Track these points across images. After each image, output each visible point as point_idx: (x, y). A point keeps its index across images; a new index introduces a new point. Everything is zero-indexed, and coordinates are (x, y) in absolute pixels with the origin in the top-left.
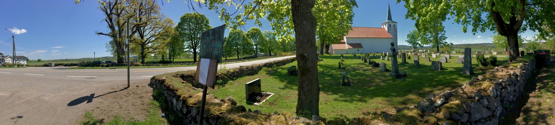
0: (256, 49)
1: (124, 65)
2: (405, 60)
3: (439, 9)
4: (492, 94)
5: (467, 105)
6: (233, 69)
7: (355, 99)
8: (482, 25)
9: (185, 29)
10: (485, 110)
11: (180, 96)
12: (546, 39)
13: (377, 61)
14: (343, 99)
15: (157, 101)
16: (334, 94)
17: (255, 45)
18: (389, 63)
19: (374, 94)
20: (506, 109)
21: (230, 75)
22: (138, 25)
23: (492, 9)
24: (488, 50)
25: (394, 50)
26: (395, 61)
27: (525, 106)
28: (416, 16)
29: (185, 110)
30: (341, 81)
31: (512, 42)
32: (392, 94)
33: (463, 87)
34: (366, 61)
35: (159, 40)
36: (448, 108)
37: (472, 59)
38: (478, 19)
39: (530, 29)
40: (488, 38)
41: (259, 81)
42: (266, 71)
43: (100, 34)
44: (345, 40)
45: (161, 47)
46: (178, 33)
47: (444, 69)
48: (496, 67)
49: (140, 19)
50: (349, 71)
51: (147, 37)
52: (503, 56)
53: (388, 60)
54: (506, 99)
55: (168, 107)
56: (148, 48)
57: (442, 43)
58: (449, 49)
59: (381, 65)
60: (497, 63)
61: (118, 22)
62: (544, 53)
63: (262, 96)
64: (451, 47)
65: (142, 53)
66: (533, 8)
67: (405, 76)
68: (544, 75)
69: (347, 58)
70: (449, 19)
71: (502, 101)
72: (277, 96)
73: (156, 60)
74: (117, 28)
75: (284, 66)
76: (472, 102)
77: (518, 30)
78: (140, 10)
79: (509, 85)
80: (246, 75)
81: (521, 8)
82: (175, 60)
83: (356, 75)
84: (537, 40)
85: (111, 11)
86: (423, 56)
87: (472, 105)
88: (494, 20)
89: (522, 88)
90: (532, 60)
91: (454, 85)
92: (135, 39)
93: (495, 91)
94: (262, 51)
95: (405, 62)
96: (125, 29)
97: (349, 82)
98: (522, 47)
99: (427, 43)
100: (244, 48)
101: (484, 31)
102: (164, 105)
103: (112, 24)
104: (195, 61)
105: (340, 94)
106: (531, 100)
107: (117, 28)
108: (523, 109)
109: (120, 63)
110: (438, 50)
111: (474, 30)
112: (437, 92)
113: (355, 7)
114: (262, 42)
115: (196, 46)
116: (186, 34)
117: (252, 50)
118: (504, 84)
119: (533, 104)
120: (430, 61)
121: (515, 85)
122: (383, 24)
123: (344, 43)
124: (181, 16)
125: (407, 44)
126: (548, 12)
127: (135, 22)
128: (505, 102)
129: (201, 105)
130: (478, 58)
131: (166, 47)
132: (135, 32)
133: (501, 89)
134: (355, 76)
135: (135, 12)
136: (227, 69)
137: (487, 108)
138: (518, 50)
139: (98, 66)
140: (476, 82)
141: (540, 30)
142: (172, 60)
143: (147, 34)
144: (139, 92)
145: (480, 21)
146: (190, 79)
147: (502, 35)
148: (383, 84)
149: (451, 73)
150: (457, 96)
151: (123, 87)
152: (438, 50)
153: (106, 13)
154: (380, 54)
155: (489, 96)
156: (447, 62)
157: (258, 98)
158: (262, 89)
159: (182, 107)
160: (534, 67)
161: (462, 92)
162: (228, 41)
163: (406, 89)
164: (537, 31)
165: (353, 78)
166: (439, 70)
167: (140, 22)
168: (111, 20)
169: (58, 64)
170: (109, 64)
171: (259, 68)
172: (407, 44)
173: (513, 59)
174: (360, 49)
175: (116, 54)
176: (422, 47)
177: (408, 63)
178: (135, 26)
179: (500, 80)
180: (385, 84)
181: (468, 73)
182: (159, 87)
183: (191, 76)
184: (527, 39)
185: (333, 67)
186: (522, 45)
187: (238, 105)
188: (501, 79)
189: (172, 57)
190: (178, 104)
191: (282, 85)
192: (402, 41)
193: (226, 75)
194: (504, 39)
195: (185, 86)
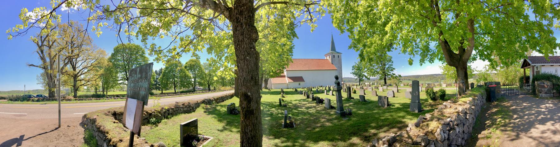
0: (195, 82)
1: (56, 100)
2: (350, 94)
3: (384, 40)
4: (439, 138)
8: (431, 55)
11: (110, 140)
12: (496, 70)
13: (321, 96)
16: (275, 138)
18: (333, 99)
21: (165, 113)
22: (70, 56)
23: (439, 39)
24: (438, 82)
25: (338, 84)
26: (340, 97)
28: (360, 46)
30: (283, 121)
31: (462, 73)
32: (337, 137)
33: (408, 129)
34: (308, 97)
35: (92, 72)
37: (421, 93)
38: (427, 49)
39: (480, 59)
40: (437, 67)
41: (195, 122)
42: (203, 108)
43: (30, 65)
44: (285, 73)
45: (94, 79)
46: (111, 64)
49: (72, 51)
50: (290, 109)
51: (80, 69)
52: (452, 90)
54: (454, 143)
56: (81, 80)
57: (389, 75)
58: (397, 82)
59: (326, 101)
62: (494, 85)
63: (198, 140)
64: (399, 78)
65: (74, 86)
66: (483, 38)
67: (350, 114)
68: (495, 110)
69: (287, 93)
70: (396, 49)
72: (217, 141)
73: (89, 93)
74: (48, 60)
75: (222, 104)
77: (468, 60)
79: (457, 125)
80: (182, 113)
81: (471, 36)
82: (109, 93)
85: (42, 42)
86: (369, 89)
88: (443, 49)
89: (471, 128)
90: (482, 94)
91: (399, 125)
92: (66, 71)
93: (442, 133)
94: (200, 84)
95: (350, 98)
96: (57, 61)
97: (291, 123)
98: (472, 78)
100: (181, 81)
101: (433, 61)
103: (44, 56)
107: (48, 60)
109: (51, 97)
110: (385, 83)
111: (422, 61)
112: (382, 135)
114: (201, 75)
116: (119, 65)
117: (190, 83)
118: (451, 123)
120: (377, 95)
121: (464, 125)
122: (326, 55)
123: (284, 76)
126: (497, 43)
127: (68, 54)
130: (427, 92)
131: (99, 79)
132: (67, 63)
133: (449, 131)
136: (160, 105)
138: (467, 82)
139: (28, 100)
140: (423, 122)
141: (490, 60)
142: (105, 93)
143: (80, 65)
144: (70, 134)
145: (428, 51)
147: (451, 65)
148: (328, 124)
149: (398, 110)
152: (385, 83)
153: (38, 44)
154: (324, 88)
156: (394, 97)
158: (199, 132)
161: (406, 136)
162: (165, 72)
163: (351, 131)
164: (487, 61)
165: (295, 117)
166: (386, 106)
168: (42, 52)
170: (40, 98)
171: (197, 105)
172: (352, 76)
173: (462, 92)
174: (302, 83)
176: (369, 79)
177: (353, 98)
178: (67, 57)
179: (449, 120)
181: (417, 112)
186: (473, 76)
188: (449, 117)
189: (105, 90)
191: (220, 125)
192: (347, 73)
193: (160, 112)
194: (453, 70)
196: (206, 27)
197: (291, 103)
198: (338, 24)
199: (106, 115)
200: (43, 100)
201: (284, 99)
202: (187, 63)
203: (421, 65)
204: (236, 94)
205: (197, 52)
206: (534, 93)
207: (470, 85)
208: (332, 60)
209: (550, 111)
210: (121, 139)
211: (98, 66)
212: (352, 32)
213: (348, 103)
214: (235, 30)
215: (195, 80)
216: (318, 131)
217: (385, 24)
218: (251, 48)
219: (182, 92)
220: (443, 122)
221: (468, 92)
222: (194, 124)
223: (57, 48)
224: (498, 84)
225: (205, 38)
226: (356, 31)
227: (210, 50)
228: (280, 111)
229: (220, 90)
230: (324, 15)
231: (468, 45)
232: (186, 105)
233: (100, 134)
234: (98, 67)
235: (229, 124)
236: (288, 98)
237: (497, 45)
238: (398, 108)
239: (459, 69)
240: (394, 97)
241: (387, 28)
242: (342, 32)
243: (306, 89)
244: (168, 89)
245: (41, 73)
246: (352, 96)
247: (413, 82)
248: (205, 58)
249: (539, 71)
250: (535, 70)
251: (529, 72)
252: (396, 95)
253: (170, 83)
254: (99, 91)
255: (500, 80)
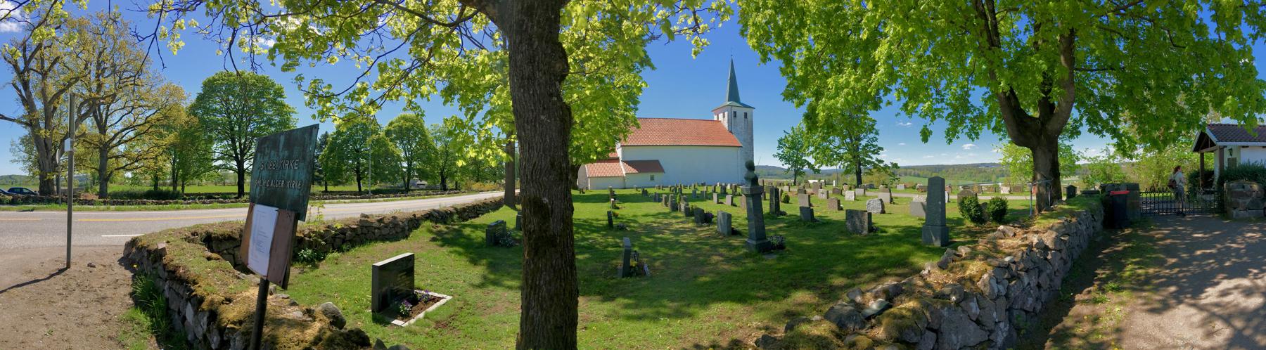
0: (409, 168)
1: (56, 201)
2: (777, 205)
4: (987, 290)
5: (931, 313)
6: (342, 221)
7: (663, 310)
9: (216, 110)
10: (973, 326)
11: (201, 300)
13: (708, 206)
14: (630, 312)
15: (144, 310)
17: (407, 159)
18: (740, 213)
19: (709, 295)
20: (1018, 330)
21: (334, 237)
22: (95, 99)
24: (989, 181)
26: (755, 209)
27: (1059, 326)
29: (215, 340)
31: (1045, 162)
32: (753, 293)
34: (675, 208)
35: (146, 138)
36: (895, 316)
37: (948, 206)
38: (962, 105)
39: (1090, 130)
40: (989, 154)
41: (410, 259)
42: (430, 232)
44: (619, 152)
46: (195, 120)
47: (877, 229)
48: (1002, 227)
49: (100, 86)
50: (635, 235)
52: (1020, 200)
53: (733, 205)
55: (173, 329)
56: (117, 157)
57: (869, 162)
58: (888, 179)
60: (1007, 216)
61: (43, 92)
62: (1123, 191)
63: (414, 301)
65: (102, 169)
67: (781, 247)
69: (625, 199)
70: (889, 103)
71: (1009, 310)
72: (460, 304)
73: (137, 189)
74: (39, 105)
75: (477, 221)
76: (944, 305)
77: (1059, 132)
78: (99, 65)
79: (1027, 271)
80: (376, 240)
82: (188, 190)
83: (655, 244)
84: (1114, 157)
85: (27, 62)
87: (945, 312)
88: (1002, 107)
89: (1058, 282)
92: (84, 135)
93: (993, 282)
94: (423, 175)
95: (776, 212)
99: (830, 162)
101: (977, 134)
102: (163, 324)
103: (29, 95)
104: (241, 192)
105: (622, 300)
106: (1077, 309)
107: (39, 105)
108: (1053, 331)
109: (46, 195)
110: (859, 181)
111: (951, 135)
113: (647, 68)
114: (424, 152)
115: (243, 154)
116: (217, 123)
117: (397, 170)
118: (1013, 267)
119: (1079, 320)
121: (1040, 272)
122: (717, 111)
123: (617, 160)
124: (204, 78)
125: (778, 163)
126: (1130, 92)
127: (86, 93)
128: (1015, 313)
129: (252, 326)
130: (962, 204)
131: (164, 157)
132: (86, 115)
134: (653, 247)
135: (86, 68)
136: (325, 219)
137: (978, 322)
141: (1115, 133)
143: (116, 122)
144: (95, 285)
146: (228, 245)
149: (896, 240)
150: (910, 294)
151: (54, 268)
153: (15, 66)
154: (710, 190)
155: (982, 294)
157: (405, 307)
158: (417, 283)
159: (208, 330)
160: (1099, 225)
162: (334, 143)
163: (787, 281)
164: (1108, 135)
166: (865, 232)
167: (98, 92)
169: (18, 286)
171: (414, 222)
172: (778, 163)
173: (1045, 204)
174: (658, 176)
175: (36, 170)
176: (818, 171)
177: (784, 214)
178: (86, 101)
179: (1007, 259)
180: (734, 268)
181: (937, 244)
182: (148, 270)
183: (229, 238)
184: (1087, 155)
185: (591, 225)
186: (1073, 170)
187: (349, 326)
188: (1009, 255)
189: (180, 182)
190: (197, 322)
191: (477, 272)
192: (766, 157)
193: (322, 236)
194: (1025, 155)
195: (214, 270)
196: (439, 41)
197: (635, 222)
198: (759, 39)
199: (187, 239)
200: (26, 201)
201: (617, 211)
202: (391, 124)
203: (950, 141)
204: (509, 200)
205: (418, 100)
206: (1222, 210)
207: (1064, 191)
208: (730, 122)
209: (1251, 248)
210: (228, 296)
211: (164, 122)
212: (789, 62)
213: (774, 224)
214: (514, 50)
215: (410, 165)
216: (706, 283)
217: (872, 43)
218: (551, 95)
219: (376, 192)
220: (995, 263)
221: (1059, 207)
222: (407, 266)
223: (62, 77)
224: (1134, 187)
225: (439, 67)
226: (799, 56)
227: (449, 92)
228: (610, 240)
229: (470, 190)
230: (727, 19)
231: (1060, 94)
232: (386, 221)
233: (176, 286)
234: (163, 126)
235: (492, 267)
236: (627, 210)
237: (1129, 96)
238: (894, 236)
239: (1039, 153)
240: (883, 212)
241: (881, 52)
242: (765, 59)
243: (667, 190)
244: (343, 184)
245: (22, 135)
246: (782, 209)
247: (930, 180)
248: (437, 115)
249: (1235, 160)
250: (1227, 156)
251: (1212, 161)
252: (888, 207)
253: (347, 170)
254: (164, 184)
255: (1144, 180)
